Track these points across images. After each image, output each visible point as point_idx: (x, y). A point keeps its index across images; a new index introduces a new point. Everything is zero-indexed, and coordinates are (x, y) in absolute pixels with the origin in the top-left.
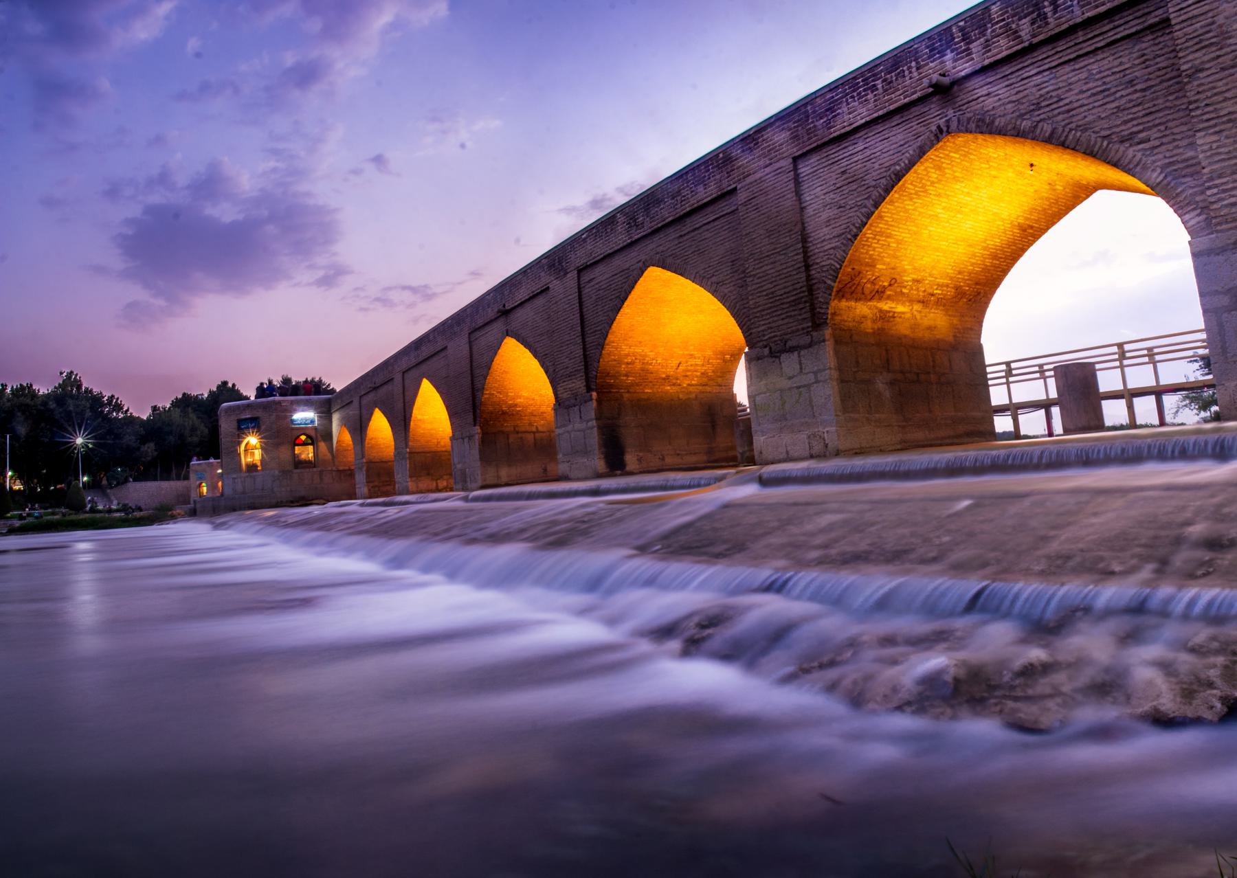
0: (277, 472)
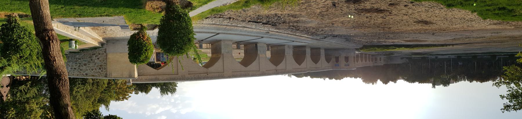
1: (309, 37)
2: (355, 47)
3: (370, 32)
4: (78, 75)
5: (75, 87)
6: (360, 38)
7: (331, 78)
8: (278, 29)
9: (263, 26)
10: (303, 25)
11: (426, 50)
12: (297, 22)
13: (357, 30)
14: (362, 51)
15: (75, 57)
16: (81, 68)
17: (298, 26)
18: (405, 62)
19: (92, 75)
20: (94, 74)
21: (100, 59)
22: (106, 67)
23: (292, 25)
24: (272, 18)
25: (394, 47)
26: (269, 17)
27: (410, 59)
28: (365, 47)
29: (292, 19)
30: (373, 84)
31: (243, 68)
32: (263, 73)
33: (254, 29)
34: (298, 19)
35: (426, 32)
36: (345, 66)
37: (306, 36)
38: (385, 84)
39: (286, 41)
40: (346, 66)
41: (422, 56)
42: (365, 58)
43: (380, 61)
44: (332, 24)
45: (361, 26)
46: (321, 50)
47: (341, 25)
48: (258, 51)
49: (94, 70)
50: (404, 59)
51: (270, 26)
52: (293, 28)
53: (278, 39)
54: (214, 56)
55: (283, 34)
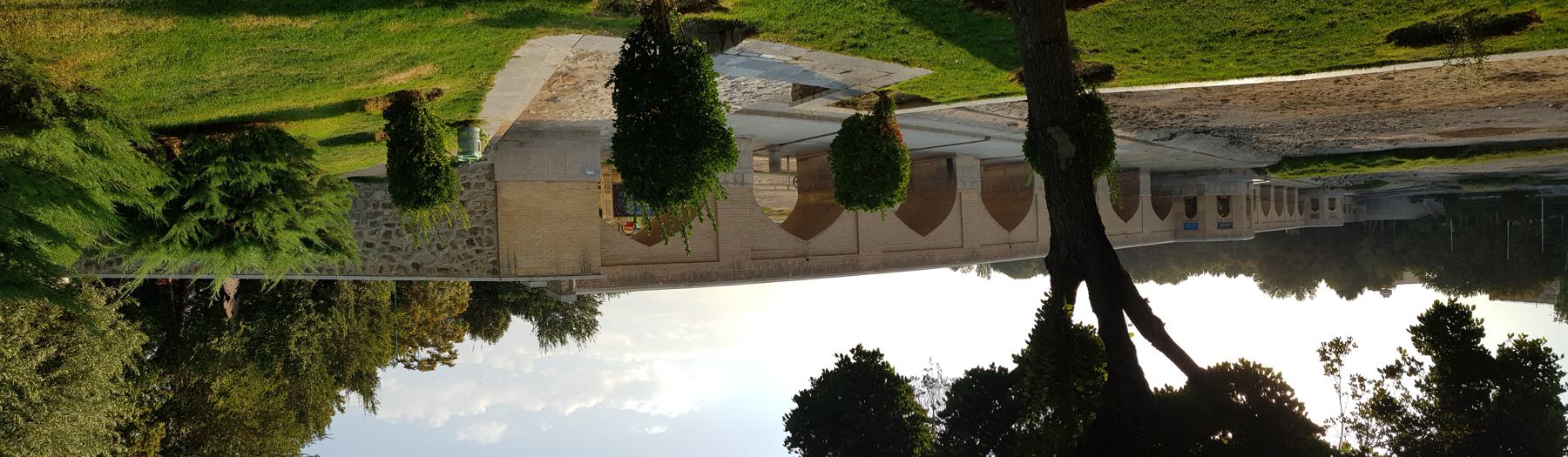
2: (1252, 163)
4: (380, 272)
5: (292, 322)
11: (1524, 164)
14: (1275, 178)
15: (369, 199)
16: (395, 241)
18: (1432, 213)
19: (440, 270)
20: (447, 265)
21: (470, 205)
22: (493, 236)
25: (1396, 157)
27: (1450, 199)
28: (1290, 162)
30: (1300, 297)
31: (791, 243)
32: (973, 255)
35: (1524, 102)
36: (1219, 227)
38: (1349, 298)
40: (1224, 228)
41: (1507, 188)
42: (1276, 200)
43: (1330, 211)
49: (446, 250)
54: (812, 198)
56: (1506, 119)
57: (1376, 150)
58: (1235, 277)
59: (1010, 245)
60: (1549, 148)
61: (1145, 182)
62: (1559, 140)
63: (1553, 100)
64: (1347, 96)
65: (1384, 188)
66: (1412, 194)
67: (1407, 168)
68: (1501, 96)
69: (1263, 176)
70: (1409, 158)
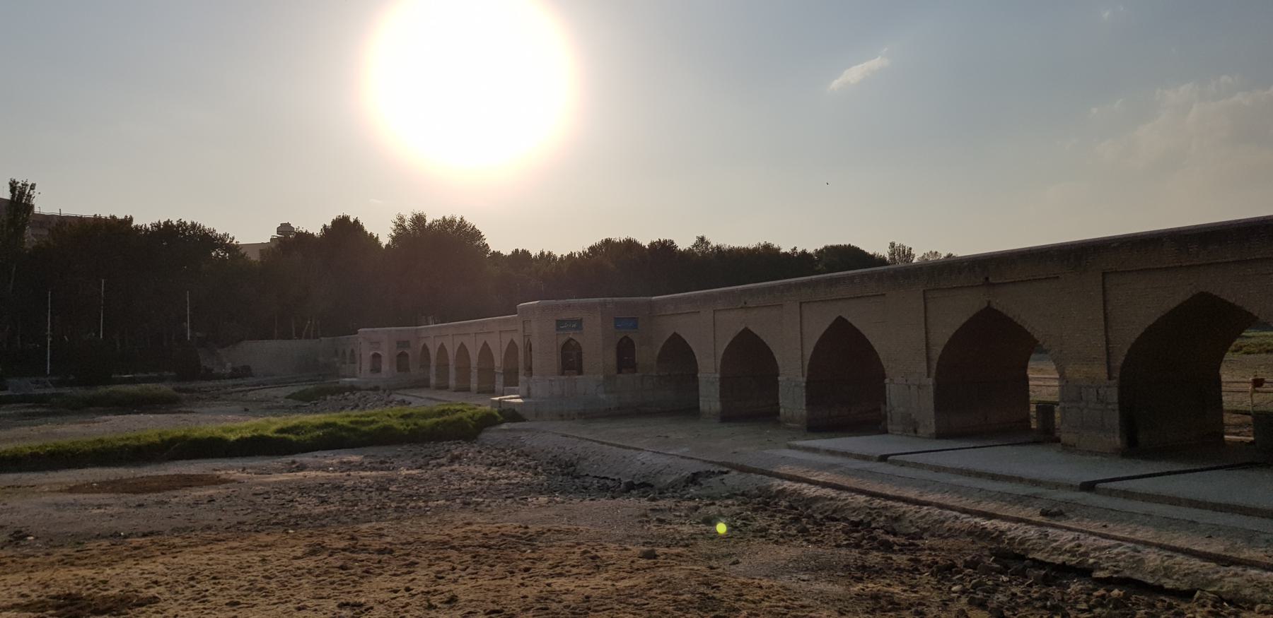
0: (602, 377)
1: (787, 484)
2: (527, 430)
3: (435, 519)
6: (493, 479)
7: (664, 249)
8: (983, 534)
9: (1086, 554)
10: (825, 552)
12: (865, 572)
13: (510, 525)
14: (485, 405)
17: (858, 546)
18: (218, 351)
23: (894, 557)
24: (1027, 603)
25: (291, 441)
26: (1045, 607)
29: (897, 589)
30: (419, 220)
33: (1147, 544)
34: (857, 588)
36: (580, 322)
37: (811, 491)
39: (932, 459)
40: (572, 321)
41: (102, 390)
44: (655, 557)
45: (490, 547)
46: (716, 406)
47: (605, 549)
48: (1115, 399)
50: (228, 368)
51: (1039, 556)
52: (891, 538)
53: (979, 475)
55: (949, 500)
56: (110, 510)
57: (325, 453)
58: (517, 250)
59: (987, 283)
60: (34, 456)
61: (710, 399)
62: (20, 471)
63: (27, 551)
64: (413, 564)
65: (295, 389)
66: (250, 380)
67: (268, 421)
68: (122, 559)
69: (503, 407)
70: (270, 438)
